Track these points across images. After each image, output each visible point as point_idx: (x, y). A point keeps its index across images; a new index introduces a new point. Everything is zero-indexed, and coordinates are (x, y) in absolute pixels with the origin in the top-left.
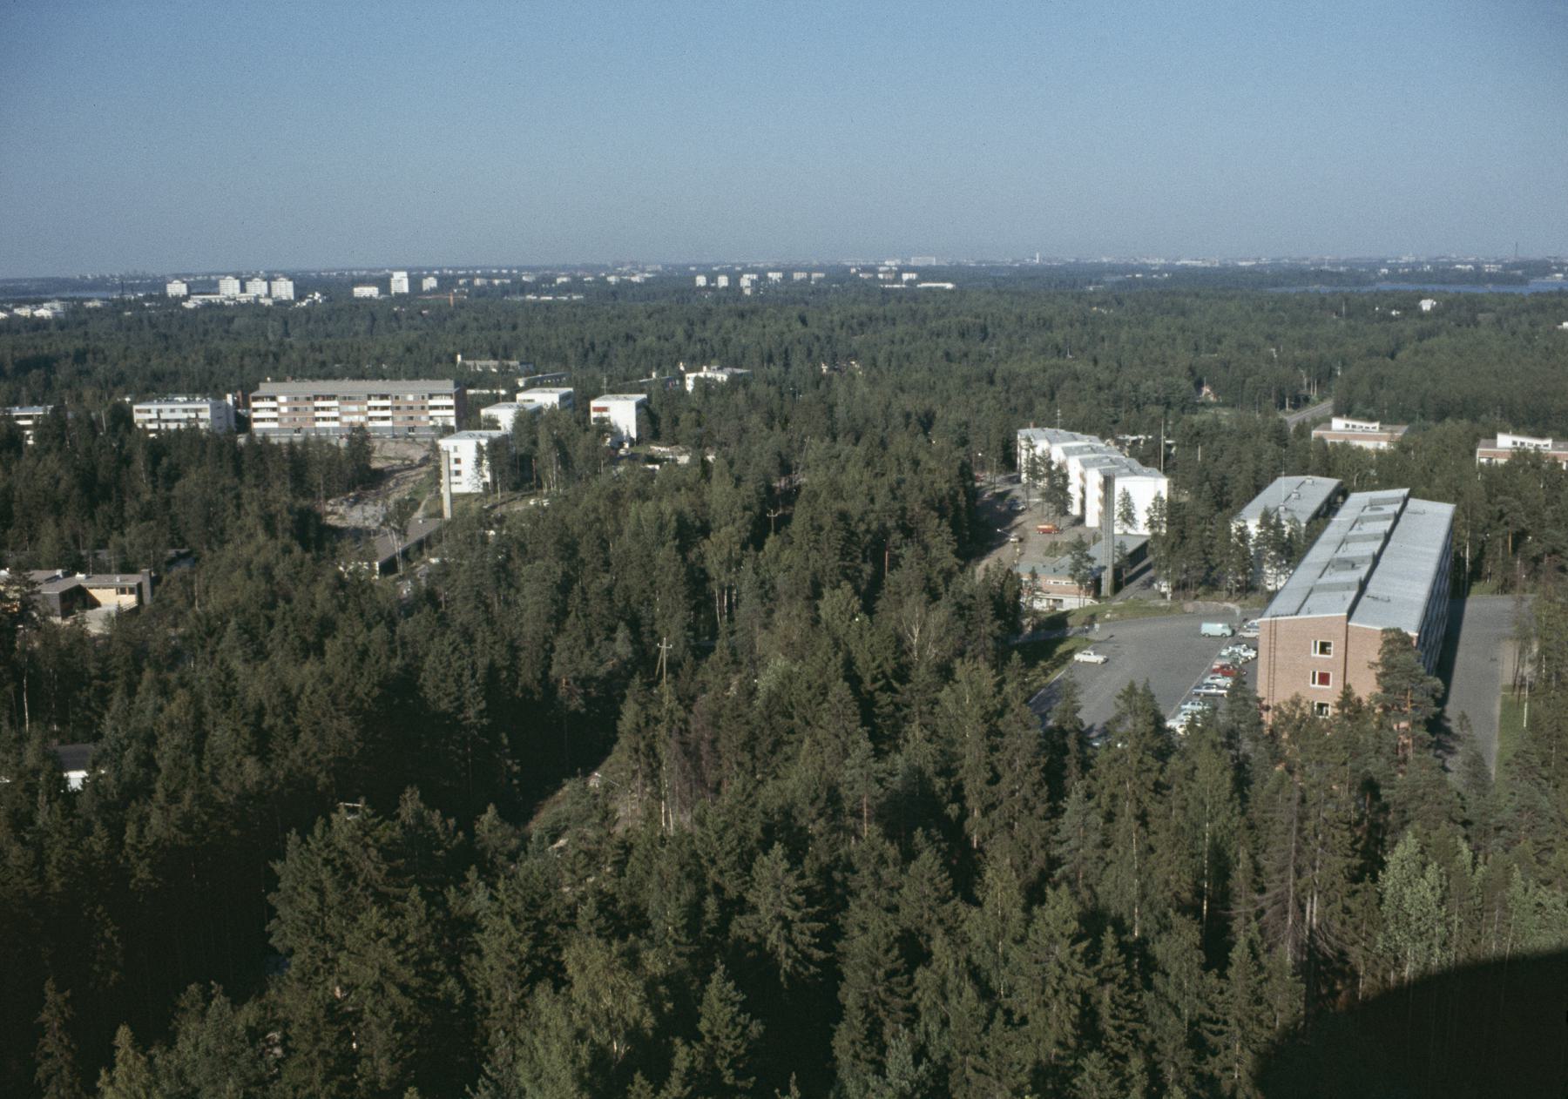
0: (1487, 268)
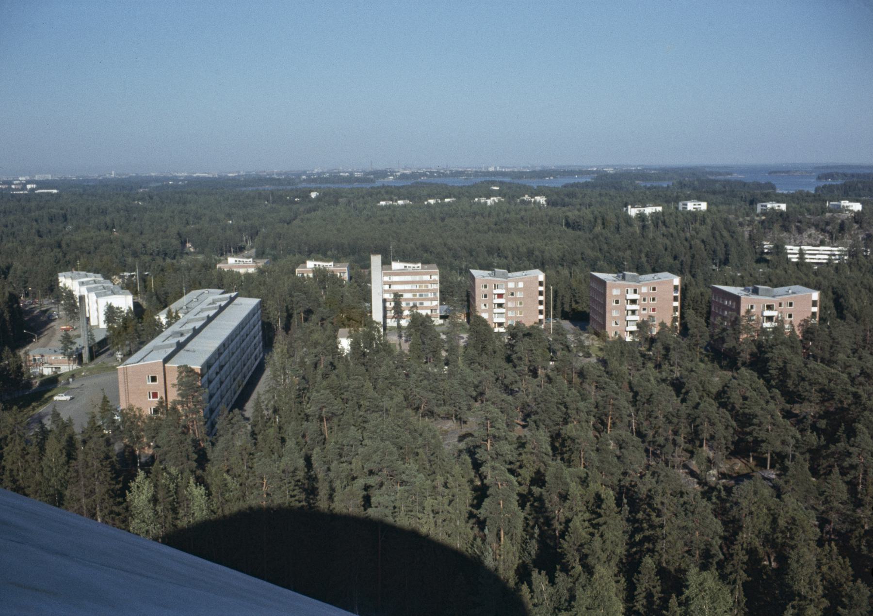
0: (357, 175)
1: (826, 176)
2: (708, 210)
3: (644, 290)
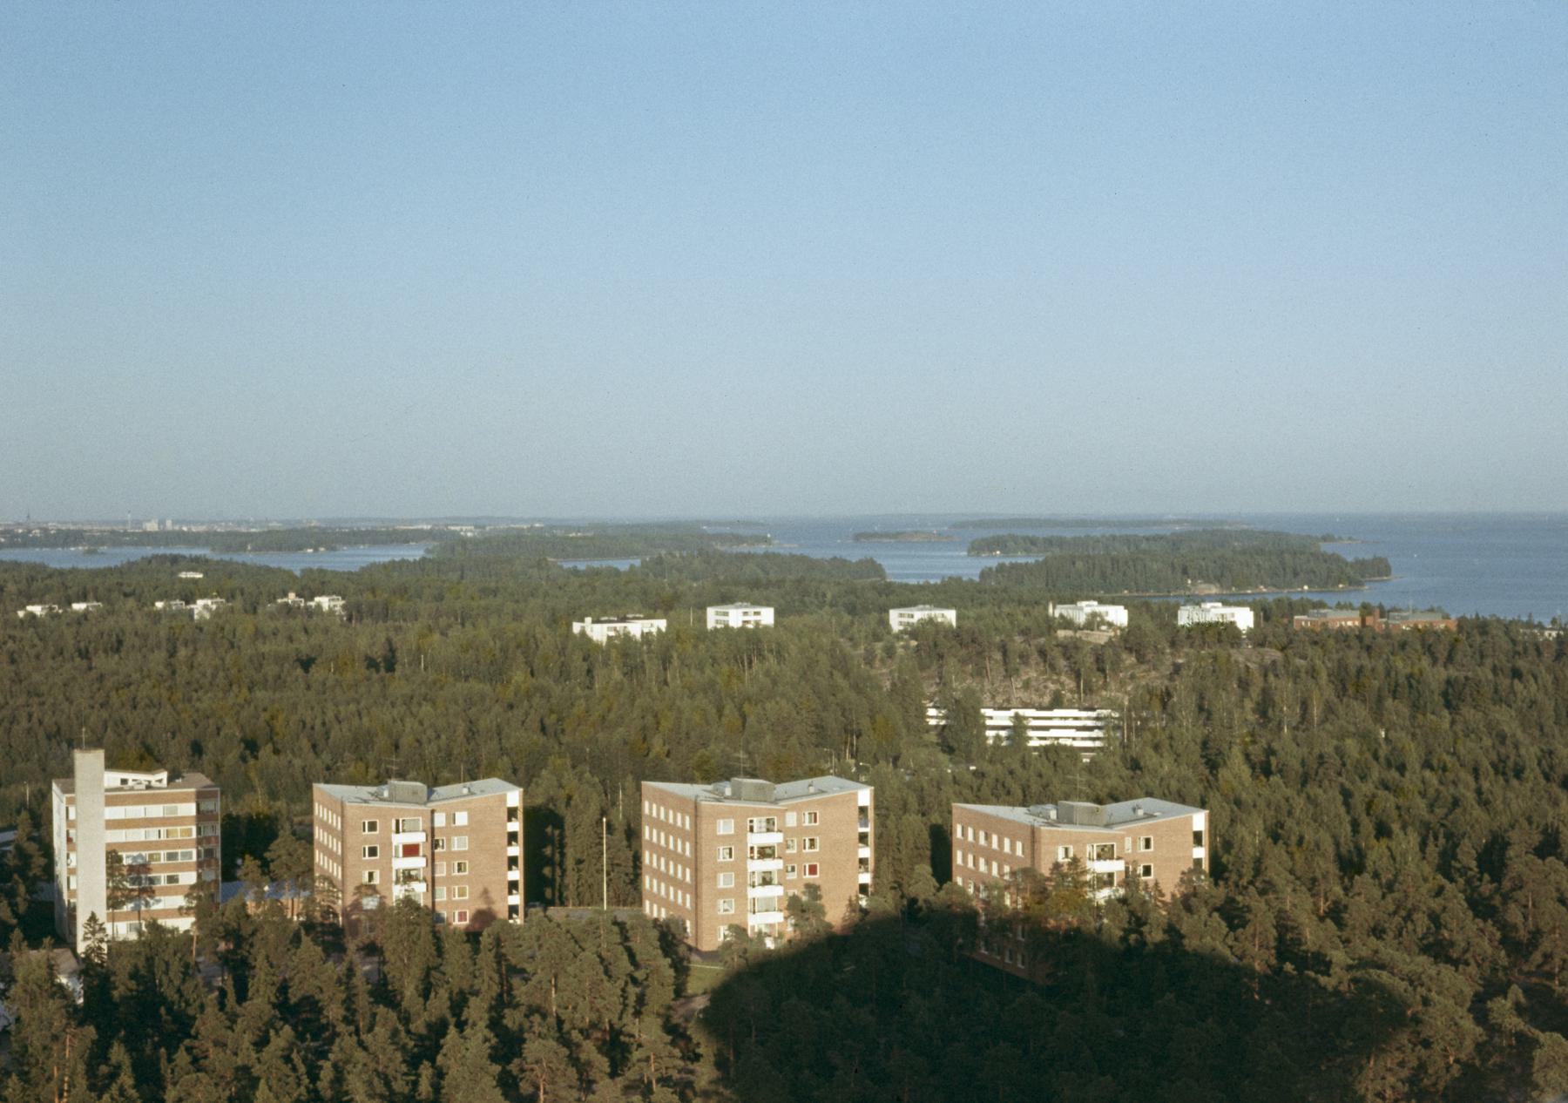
3: (791, 819)
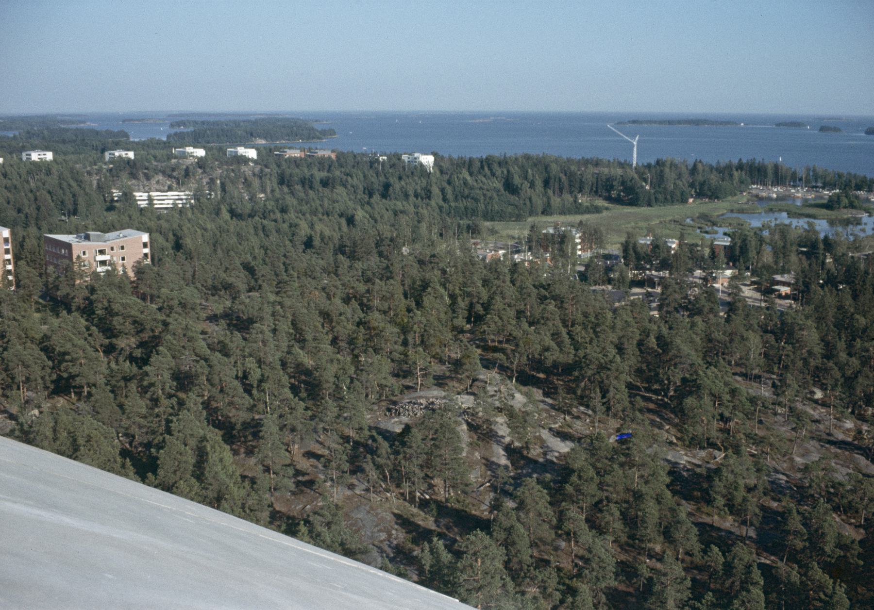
1: (179, 124)
2: (55, 160)
